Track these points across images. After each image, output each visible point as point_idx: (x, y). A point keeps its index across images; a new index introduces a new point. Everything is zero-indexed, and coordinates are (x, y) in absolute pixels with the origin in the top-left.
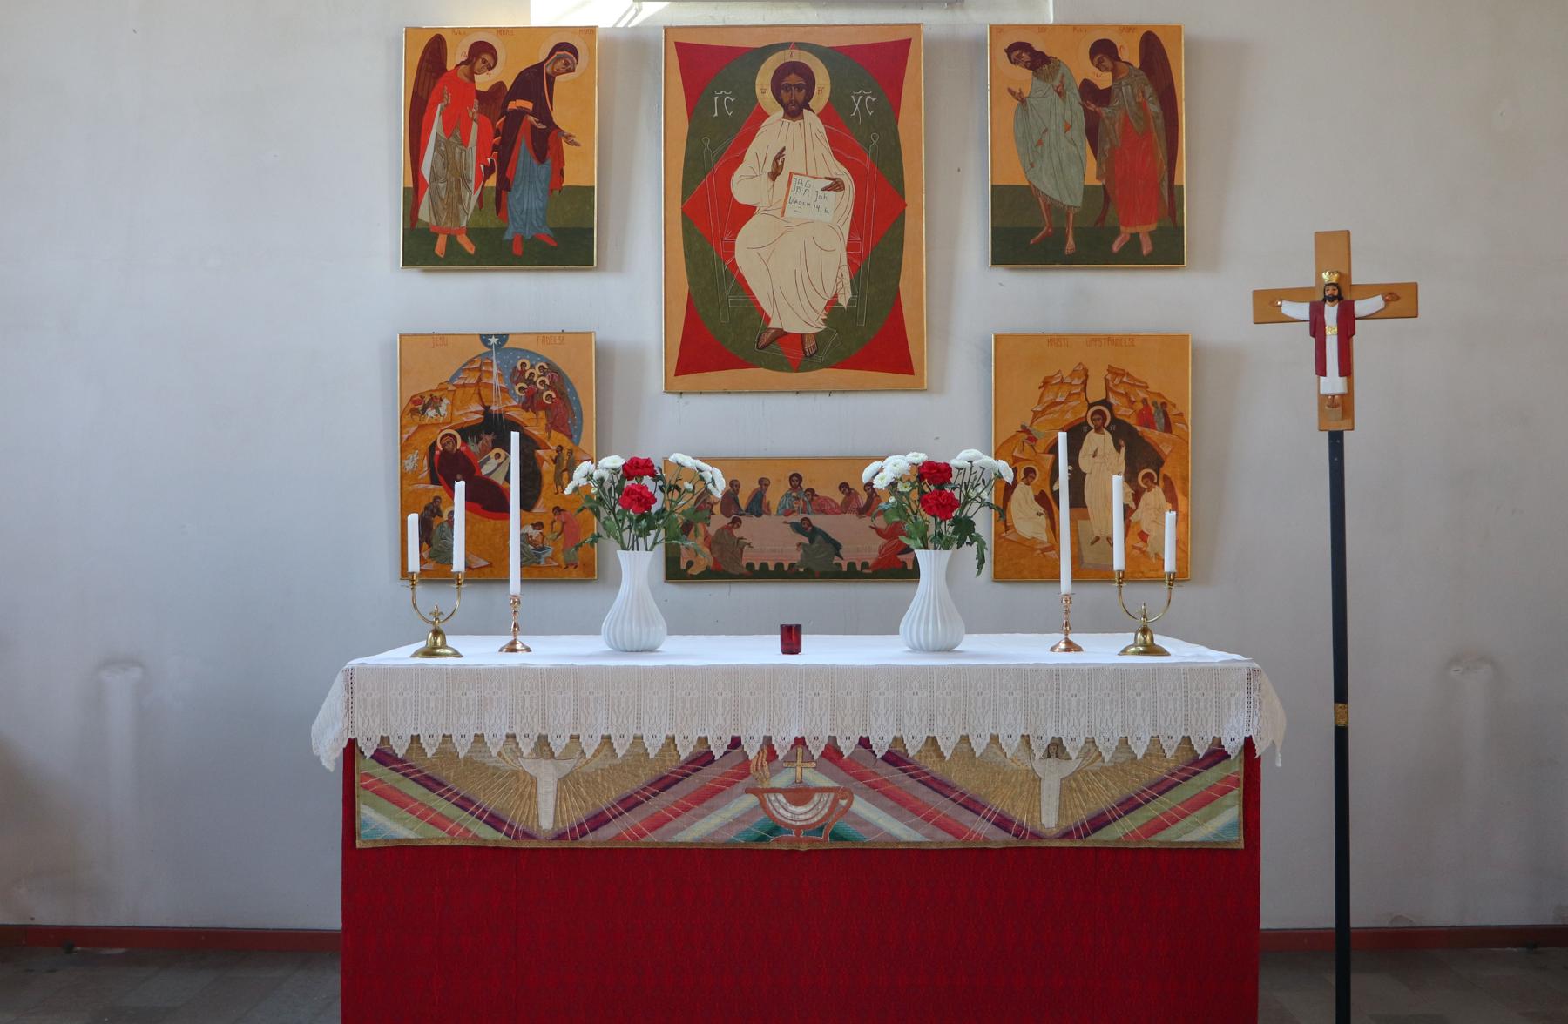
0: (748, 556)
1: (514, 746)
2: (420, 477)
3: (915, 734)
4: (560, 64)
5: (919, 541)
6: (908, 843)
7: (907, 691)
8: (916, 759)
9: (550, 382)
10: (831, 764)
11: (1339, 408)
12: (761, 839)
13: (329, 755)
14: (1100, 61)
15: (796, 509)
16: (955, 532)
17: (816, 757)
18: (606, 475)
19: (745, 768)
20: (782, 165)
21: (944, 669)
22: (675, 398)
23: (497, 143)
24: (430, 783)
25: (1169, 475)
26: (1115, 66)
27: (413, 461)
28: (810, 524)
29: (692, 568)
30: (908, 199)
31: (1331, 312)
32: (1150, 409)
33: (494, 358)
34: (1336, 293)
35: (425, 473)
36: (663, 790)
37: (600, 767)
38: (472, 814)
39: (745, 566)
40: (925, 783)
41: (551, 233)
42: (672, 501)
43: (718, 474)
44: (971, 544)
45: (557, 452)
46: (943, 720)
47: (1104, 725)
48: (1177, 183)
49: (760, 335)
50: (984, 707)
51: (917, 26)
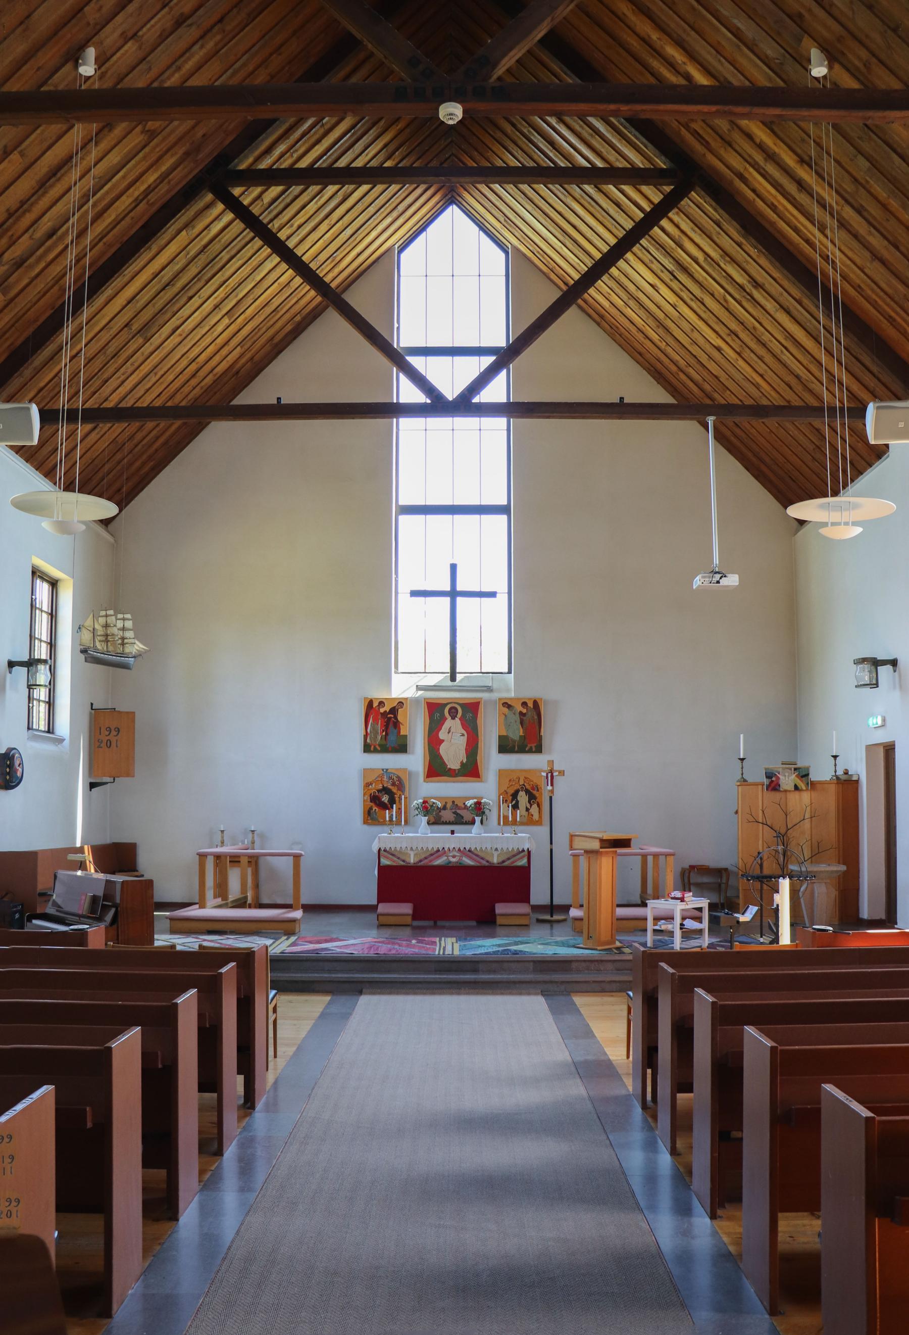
0: (442, 820)
13: (375, 850)
19: (445, 852)
31: (549, 775)
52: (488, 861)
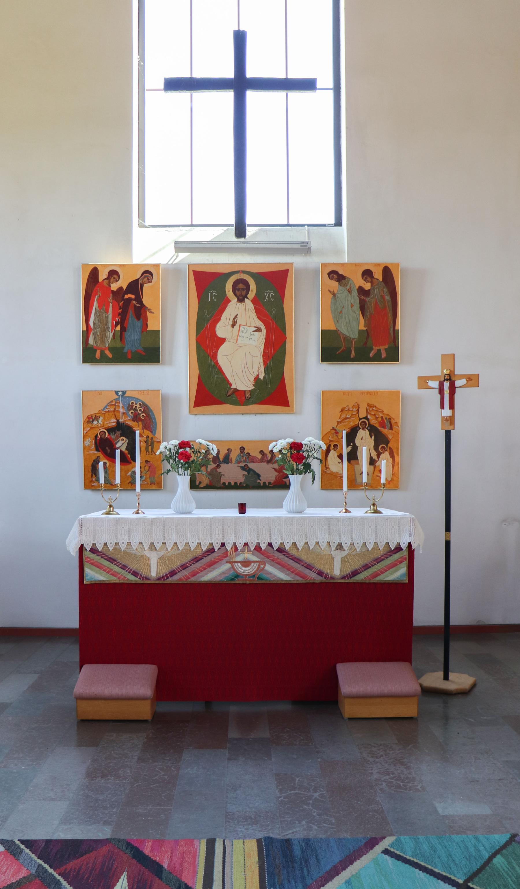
0: (223, 480)
1: (142, 546)
2: (91, 448)
3: (288, 541)
4: (145, 279)
5: (290, 472)
6: (286, 581)
7: (286, 526)
8: (289, 550)
9: (143, 410)
10: (257, 552)
11: (449, 422)
12: (232, 579)
13: (74, 552)
14: (366, 278)
15: (242, 461)
16: (304, 468)
17: (252, 550)
18: (172, 447)
20: (237, 321)
21: (299, 518)
22: (193, 416)
23: (121, 312)
24: (111, 560)
25: (391, 447)
26: (372, 280)
27: (88, 442)
28: (248, 467)
29: (201, 484)
30: (288, 335)
31: (447, 385)
32: (384, 421)
33: (120, 400)
34: (449, 378)
35: (93, 446)
36: (196, 562)
37: (173, 554)
38: (127, 571)
39: (222, 483)
40: (292, 559)
41: (143, 350)
42: (197, 457)
43: (215, 447)
44: (310, 473)
45: (146, 438)
46: (299, 536)
47: (357, 538)
48: (396, 328)
49: (228, 391)
50: (313, 532)
51: (291, 264)
52: (320, 573)
